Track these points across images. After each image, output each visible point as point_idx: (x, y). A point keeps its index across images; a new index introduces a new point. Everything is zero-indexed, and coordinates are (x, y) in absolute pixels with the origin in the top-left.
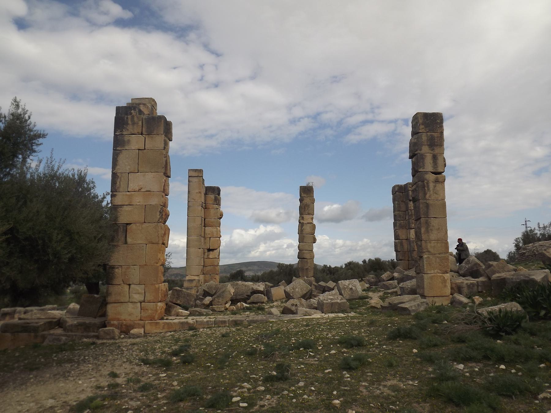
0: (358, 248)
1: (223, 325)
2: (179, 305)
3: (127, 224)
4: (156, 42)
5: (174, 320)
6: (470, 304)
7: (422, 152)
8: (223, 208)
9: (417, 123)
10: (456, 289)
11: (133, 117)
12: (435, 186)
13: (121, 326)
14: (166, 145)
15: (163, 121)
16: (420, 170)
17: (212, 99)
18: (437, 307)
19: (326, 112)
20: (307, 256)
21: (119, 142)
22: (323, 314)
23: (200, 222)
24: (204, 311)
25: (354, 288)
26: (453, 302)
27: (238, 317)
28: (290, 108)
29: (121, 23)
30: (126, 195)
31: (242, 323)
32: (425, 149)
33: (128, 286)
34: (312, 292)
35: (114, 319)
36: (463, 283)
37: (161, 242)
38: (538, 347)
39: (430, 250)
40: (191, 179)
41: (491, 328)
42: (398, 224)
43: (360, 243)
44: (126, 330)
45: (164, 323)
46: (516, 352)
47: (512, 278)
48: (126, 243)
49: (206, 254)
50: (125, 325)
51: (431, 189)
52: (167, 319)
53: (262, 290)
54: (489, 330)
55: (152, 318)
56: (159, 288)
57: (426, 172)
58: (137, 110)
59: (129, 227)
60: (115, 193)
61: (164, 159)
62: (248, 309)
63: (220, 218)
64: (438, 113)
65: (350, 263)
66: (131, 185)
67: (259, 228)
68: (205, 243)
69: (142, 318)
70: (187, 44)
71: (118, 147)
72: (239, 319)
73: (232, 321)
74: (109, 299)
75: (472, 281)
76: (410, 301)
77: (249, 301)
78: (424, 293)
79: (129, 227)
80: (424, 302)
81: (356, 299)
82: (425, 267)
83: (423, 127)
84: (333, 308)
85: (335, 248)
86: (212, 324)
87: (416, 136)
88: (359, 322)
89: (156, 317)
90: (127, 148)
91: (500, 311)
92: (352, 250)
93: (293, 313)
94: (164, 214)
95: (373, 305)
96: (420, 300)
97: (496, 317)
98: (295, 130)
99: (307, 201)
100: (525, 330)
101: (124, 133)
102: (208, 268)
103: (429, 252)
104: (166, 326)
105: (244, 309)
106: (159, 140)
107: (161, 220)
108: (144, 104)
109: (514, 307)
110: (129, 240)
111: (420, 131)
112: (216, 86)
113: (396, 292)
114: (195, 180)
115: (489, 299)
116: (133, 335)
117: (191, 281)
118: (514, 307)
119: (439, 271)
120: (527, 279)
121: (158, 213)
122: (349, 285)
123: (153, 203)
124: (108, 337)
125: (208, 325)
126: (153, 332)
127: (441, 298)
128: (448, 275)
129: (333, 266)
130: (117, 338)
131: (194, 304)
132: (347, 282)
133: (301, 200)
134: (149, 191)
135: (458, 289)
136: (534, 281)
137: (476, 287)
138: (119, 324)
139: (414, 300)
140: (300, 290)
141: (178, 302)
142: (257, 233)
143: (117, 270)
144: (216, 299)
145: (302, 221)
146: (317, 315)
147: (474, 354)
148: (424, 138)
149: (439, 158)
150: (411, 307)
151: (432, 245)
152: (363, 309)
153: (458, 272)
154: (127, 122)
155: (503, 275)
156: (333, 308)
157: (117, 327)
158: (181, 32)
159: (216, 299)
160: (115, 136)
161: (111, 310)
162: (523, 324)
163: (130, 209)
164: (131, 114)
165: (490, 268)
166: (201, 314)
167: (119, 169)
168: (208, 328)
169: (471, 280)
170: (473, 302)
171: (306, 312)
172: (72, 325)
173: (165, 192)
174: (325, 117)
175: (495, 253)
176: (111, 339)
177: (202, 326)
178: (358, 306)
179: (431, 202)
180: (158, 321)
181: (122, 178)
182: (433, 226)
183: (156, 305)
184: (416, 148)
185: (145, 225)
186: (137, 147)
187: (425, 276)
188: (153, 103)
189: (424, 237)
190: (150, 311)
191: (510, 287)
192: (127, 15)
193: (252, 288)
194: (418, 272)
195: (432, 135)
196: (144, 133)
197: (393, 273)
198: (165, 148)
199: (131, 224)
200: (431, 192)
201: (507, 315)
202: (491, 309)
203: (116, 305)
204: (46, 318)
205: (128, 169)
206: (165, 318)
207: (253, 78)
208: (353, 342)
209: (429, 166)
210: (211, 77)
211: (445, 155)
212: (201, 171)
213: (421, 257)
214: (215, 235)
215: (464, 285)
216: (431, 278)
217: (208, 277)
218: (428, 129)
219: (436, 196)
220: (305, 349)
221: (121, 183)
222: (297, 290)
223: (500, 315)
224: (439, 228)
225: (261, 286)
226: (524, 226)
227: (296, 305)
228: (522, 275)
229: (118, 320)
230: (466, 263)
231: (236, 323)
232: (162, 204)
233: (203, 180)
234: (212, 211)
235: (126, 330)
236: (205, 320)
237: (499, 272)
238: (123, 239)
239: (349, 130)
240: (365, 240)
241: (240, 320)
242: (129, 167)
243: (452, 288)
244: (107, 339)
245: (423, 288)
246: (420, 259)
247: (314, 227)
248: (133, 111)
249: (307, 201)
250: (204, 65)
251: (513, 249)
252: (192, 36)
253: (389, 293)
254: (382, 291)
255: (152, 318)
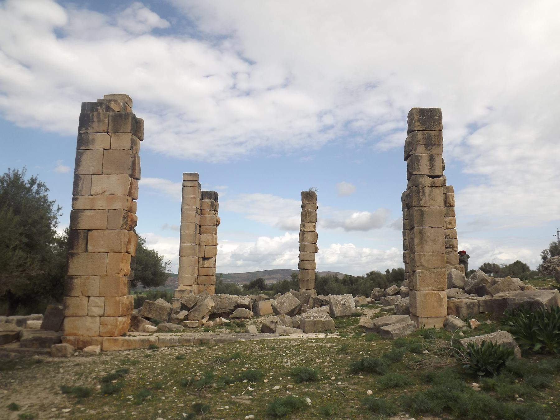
0: (386, 257)
1: (188, 344)
2: (148, 319)
3: (89, 230)
4: (191, 50)
5: (137, 336)
6: (465, 329)
7: (418, 152)
8: (220, 214)
9: (412, 120)
10: (454, 309)
11: (99, 114)
12: (431, 192)
13: (78, 342)
14: (134, 144)
15: (130, 118)
16: (414, 173)
17: (243, 107)
18: (426, 331)
19: (357, 120)
20: (308, 266)
21: (83, 141)
22: (304, 334)
23: (194, 229)
24: (174, 326)
25: (346, 304)
26: (446, 325)
27: (207, 336)
28: (320, 115)
29: (157, 32)
30: (89, 198)
31: (208, 343)
32: (421, 149)
33: (87, 299)
34: (301, 308)
35: (70, 335)
36: (461, 302)
37: (124, 250)
38: (520, 397)
39: (424, 264)
40: (186, 183)
41: (469, 366)
42: (407, 234)
43: (388, 252)
44: (80, 346)
45: (123, 340)
46: (485, 406)
47: (514, 300)
48: (86, 251)
49: (201, 263)
50: (82, 341)
51: (427, 194)
52: (130, 336)
53: (247, 303)
54: (465, 369)
55: (111, 335)
56: (119, 301)
57: (422, 176)
58: (104, 107)
59: (90, 233)
60: (76, 196)
61: (131, 160)
62: (226, 325)
63: (217, 225)
64: (436, 108)
65: (372, 273)
66: (94, 188)
67: (284, 235)
68: (200, 251)
69: (101, 334)
70: (222, 53)
71: (82, 146)
72: (205, 337)
73: (197, 340)
74: (68, 312)
75: (472, 301)
76: (397, 322)
77: (231, 316)
78: (416, 313)
79: (90, 233)
80: (410, 325)
81: (348, 316)
82: (418, 284)
83: (419, 124)
84: (317, 327)
85: (362, 257)
86: (175, 343)
87: (411, 135)
88: (331, 347)
89: (116, 334)
90: (91, 147)
91: (484, 342)
92: (378, 259)
93: (272, 331)
94: (129, 219)
95: (362, 324)
96: (410, 321)
97: (477, 352)
98: (324, 138)
99: (309, 207)
100: (510, 370)
101: (89, 131)
102: (204, 278)
103: (422, 265)
104: (125, 344)
105: (222, 324)
106: (125, 140)
107: (125, 227)
108: (115, 101)
109: (502, 337)
110: (90, 248)
111: (416, 129)
112: (248, 93)
113: (392, 309)
114: (189, 184)
115: (489, 322)
116: (87, 353)
117: (182, 291)
118: (502, 337)
119: (435, 289)
120: (530, 300)
121: (122, 219)
122: (342, 300)
123: (117, 208)
124: (60, 354)
125: (171, 343)
126: (111, 350)
127: (436, 319)
128: (444, 292)
129: (355, 275)
130: (69, 356)
131: (167, 318)
132: (339, 297)
133: (303, 207)
134: (113, 195)
135: (455, 310)
136: (539, 304)
137: (477, 307)
138: (75, 340)
139: (402, 321)
140: (288, 305)
141: (150, 316)
142: (256, 239)
143: (75, 281)
144: (192, 313)
145: (303, 229)
146: (296, 335)
147: (431, 404)
148: (420, 136)
149: (437, 159)
150: (395, 330)
151: (427, 258)
152: (352, 328)
153: (463, 289)
154: (93, 119)
155: (506, 294)
156: (317, 327)
157: (72, 343)
158: (217, 40)
159: (192, 313)
160: (80, 134)
161: (68, 324)
162: (507, 363)
163: (92, 214)
164: (97, 110)
165: (494, 286)
166: (170, 330)
167: (83, 170)
168: (171, 347)
169: (475, 299)
170: (469, 326)
171: (285, 331)
172: (26, 340)
173: (132, 195)
174: (357, 124)
175: (525, 265)
176: (62, 356)
177: (165, 345)
178: (348, 325)
179: (426, 209)
180: (117, 338)
181: (85, 180)
182: (428, 236)
183: (117, 320)
184: (411, 148)
185: (107, 232)
186: (102, 146)
187: (418, 294)
188: (126, 100)
189: (417, 248)
190: (109, 327)
191: (512, 309)
192: (164, 24)
193: (236, 302)
194: (411, 288)
195: (428, 134)
196: (110, 131)
197: (399, 286)
198: (132, 148)
199: (92, 230)
200: (427, 198)
201: (490, 349)
202: (477, 339)
203: (73, 318)
204: (4, 331)
205: (91, 170)
206: (128, 333)
207: (286, 85)
208: (303, 375)
209: (424, 168)
210: (243, 85)
211: (444, 156)
212: (196, 175)
213: (414, 272)
214: (211, 243)
215: (463, 305)
216: (425, 296)
217: (202, 287)
218: (425, 124)
219: (433, 203)
220: (249, 381)
221: (84, 186)
222: (285, 304)
223: (481, 349)
224: (435, 239)
225: (246, 300)
226: (557, 237)
227: (276, 322)
228: (526, 296)
229: (75, 335)
230: (473, 279)
231: (202, 342)
232: (126, 209)
233: (199, 184)
234: (208, 218)
235: (80, 346)
236: (168, 338)
237: (503, 291)
238: (83, 246)
239: (380, 138)
240: (393, 249)
241: (206, 339)
242: (93, 168)
243: (448, 308)
244: (59, 357)
245: (416, 307)
246: (413, 274)
247: (316, 235)
248: (99, 108)
249: (309, 207)
250: (236, 73)
251: (540, 261)
252: (227, 44)
253: (385, 310)
254: (380, 307)
255: (111, 335)
